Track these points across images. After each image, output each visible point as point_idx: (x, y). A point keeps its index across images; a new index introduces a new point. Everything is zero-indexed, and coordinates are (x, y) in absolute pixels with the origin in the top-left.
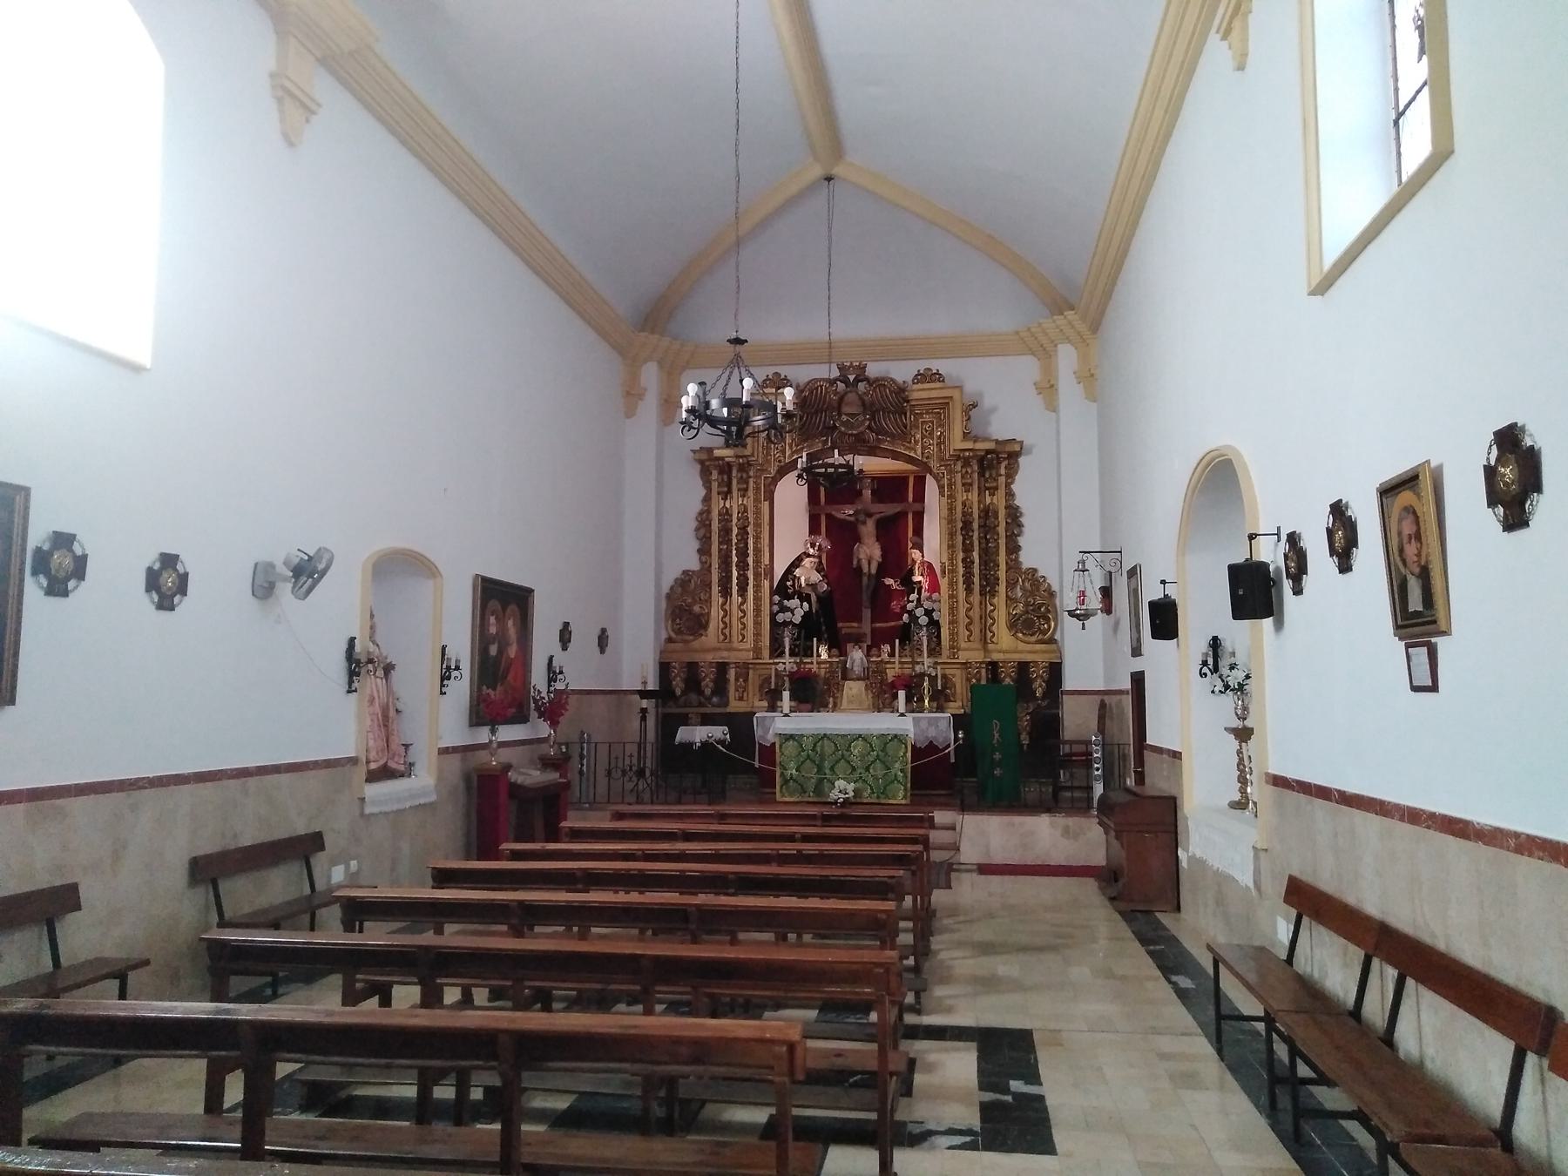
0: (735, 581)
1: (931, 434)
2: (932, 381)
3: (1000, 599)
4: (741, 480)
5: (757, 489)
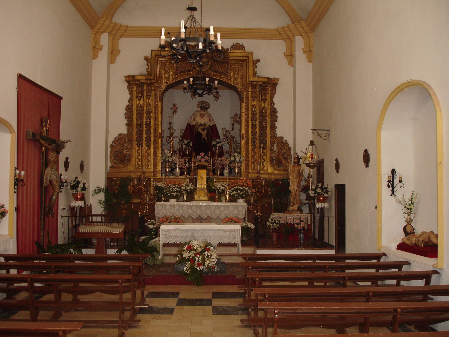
0: (144, 139)
1: (238, 73)
2: (239, 49)
3: (267, 151)
4: (148, 91)
5: (155, 96)
